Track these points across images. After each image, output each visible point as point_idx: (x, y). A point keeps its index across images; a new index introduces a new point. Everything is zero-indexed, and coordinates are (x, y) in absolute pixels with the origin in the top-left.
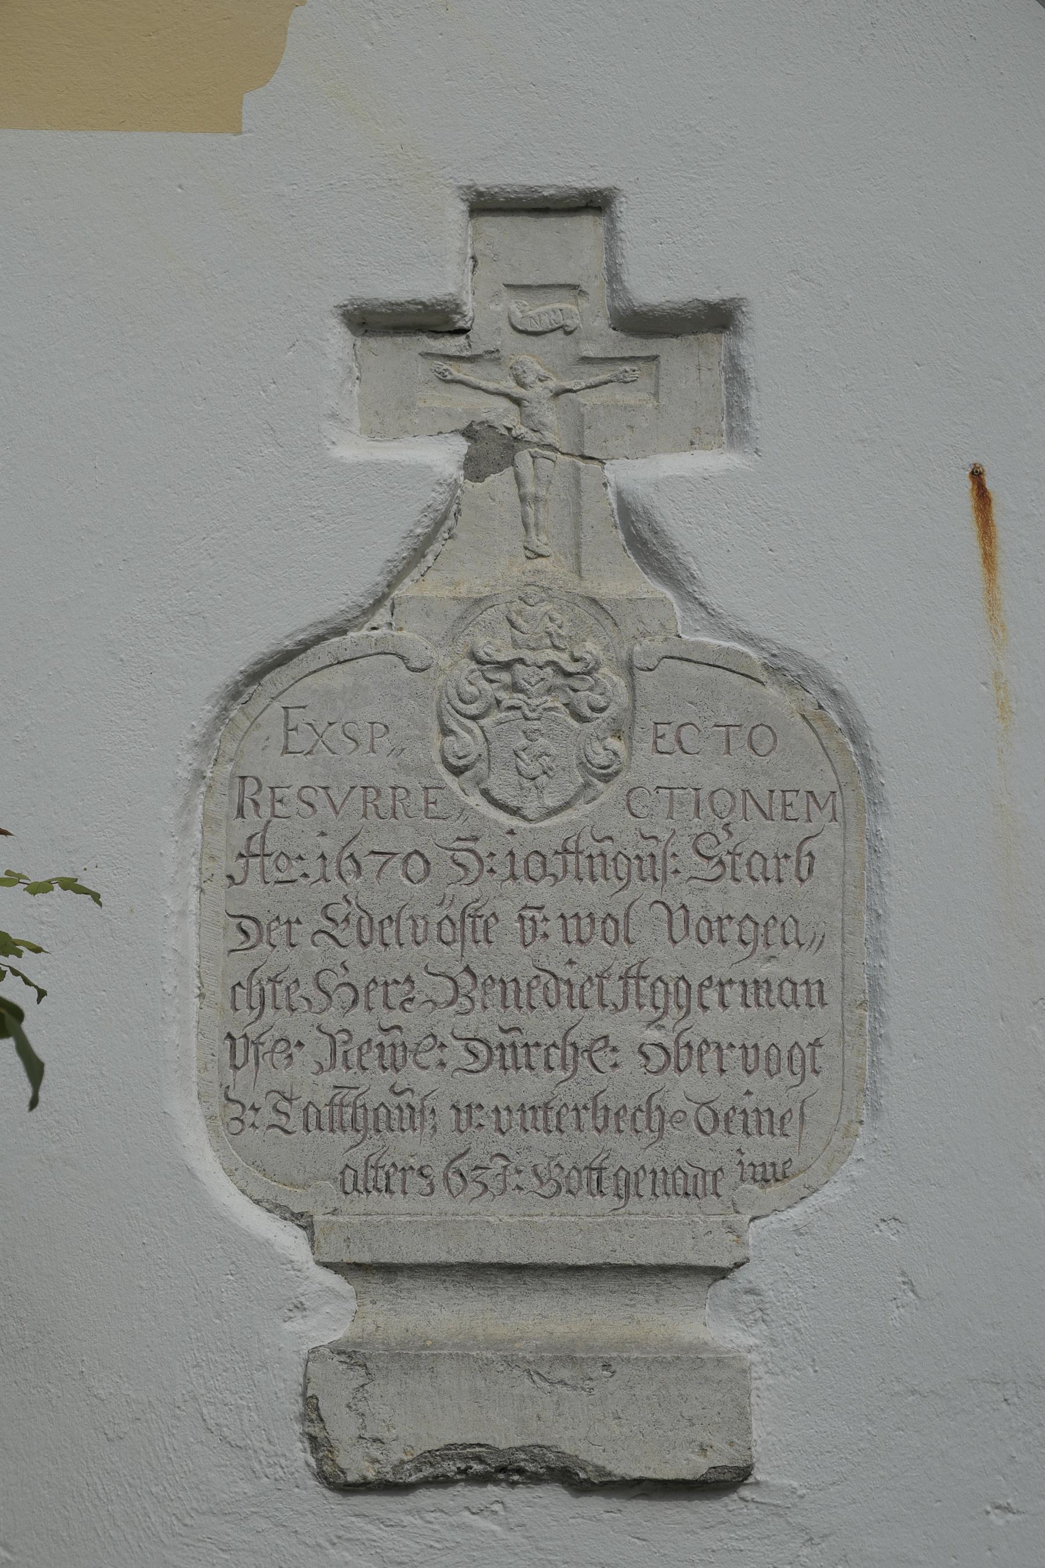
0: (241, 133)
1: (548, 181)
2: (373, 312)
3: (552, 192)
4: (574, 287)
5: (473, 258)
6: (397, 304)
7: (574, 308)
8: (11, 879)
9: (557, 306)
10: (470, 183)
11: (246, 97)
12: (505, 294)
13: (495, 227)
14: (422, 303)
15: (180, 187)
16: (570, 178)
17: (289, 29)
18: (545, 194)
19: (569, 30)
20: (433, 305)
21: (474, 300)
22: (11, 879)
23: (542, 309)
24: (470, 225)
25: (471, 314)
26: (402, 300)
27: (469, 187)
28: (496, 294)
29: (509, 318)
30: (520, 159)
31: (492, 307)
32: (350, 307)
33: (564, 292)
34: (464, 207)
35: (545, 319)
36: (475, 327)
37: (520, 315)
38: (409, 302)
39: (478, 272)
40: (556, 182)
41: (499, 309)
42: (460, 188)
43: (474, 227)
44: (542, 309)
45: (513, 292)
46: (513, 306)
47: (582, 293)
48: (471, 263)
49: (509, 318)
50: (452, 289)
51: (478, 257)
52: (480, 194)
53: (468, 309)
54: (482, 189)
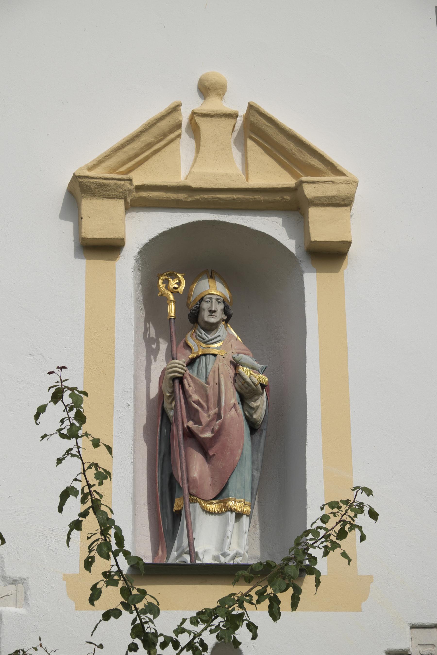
0: (361, 612)
1: (427, 622)
2: (392, 651)
3: (428, 624)
4: (433, 645)
5: (411, 638)
6: (397, 650)
7: (433, 649)
8: (94, 654)
9: (429, 649)
10: (411, 622)
11: (362, 604)
12: (418, 646)
13: (415, 631)
14: (402, 650)
15: (349, 624)
16: (432, 621)
17: (370, 588)
18: (427, 624)
19: (430, 588)
20: (405, 650)
21: (412, 648)
22: (94, 654)
23: (426, 650)
24: (238, 458)
25: (411, 651)
26: (398, 649)
27: (411, 623)
28: (417, 646)
29: (419, 652)
30: (421, 617)
31: (416, 649)
32: (387, 651)
33: (431, 646)
34: (409, 627)
35: (427, 652)
36: (412, 654)
37: (422, 651)
38: (399, 649)
39: (412, 641)
40: (429, 622)
41: (417, 650)
42: (409, 623)
43: (411, 631)
44: (426, 650)
45: (420, 646)
46: (420, 649)
47: (435, 646)
48: (410, 639)
49: (419, 652)
50: (408, 646)
51: (412, 638)
52: (413, 625)
53: (411, 650)
54: (413, 624)
